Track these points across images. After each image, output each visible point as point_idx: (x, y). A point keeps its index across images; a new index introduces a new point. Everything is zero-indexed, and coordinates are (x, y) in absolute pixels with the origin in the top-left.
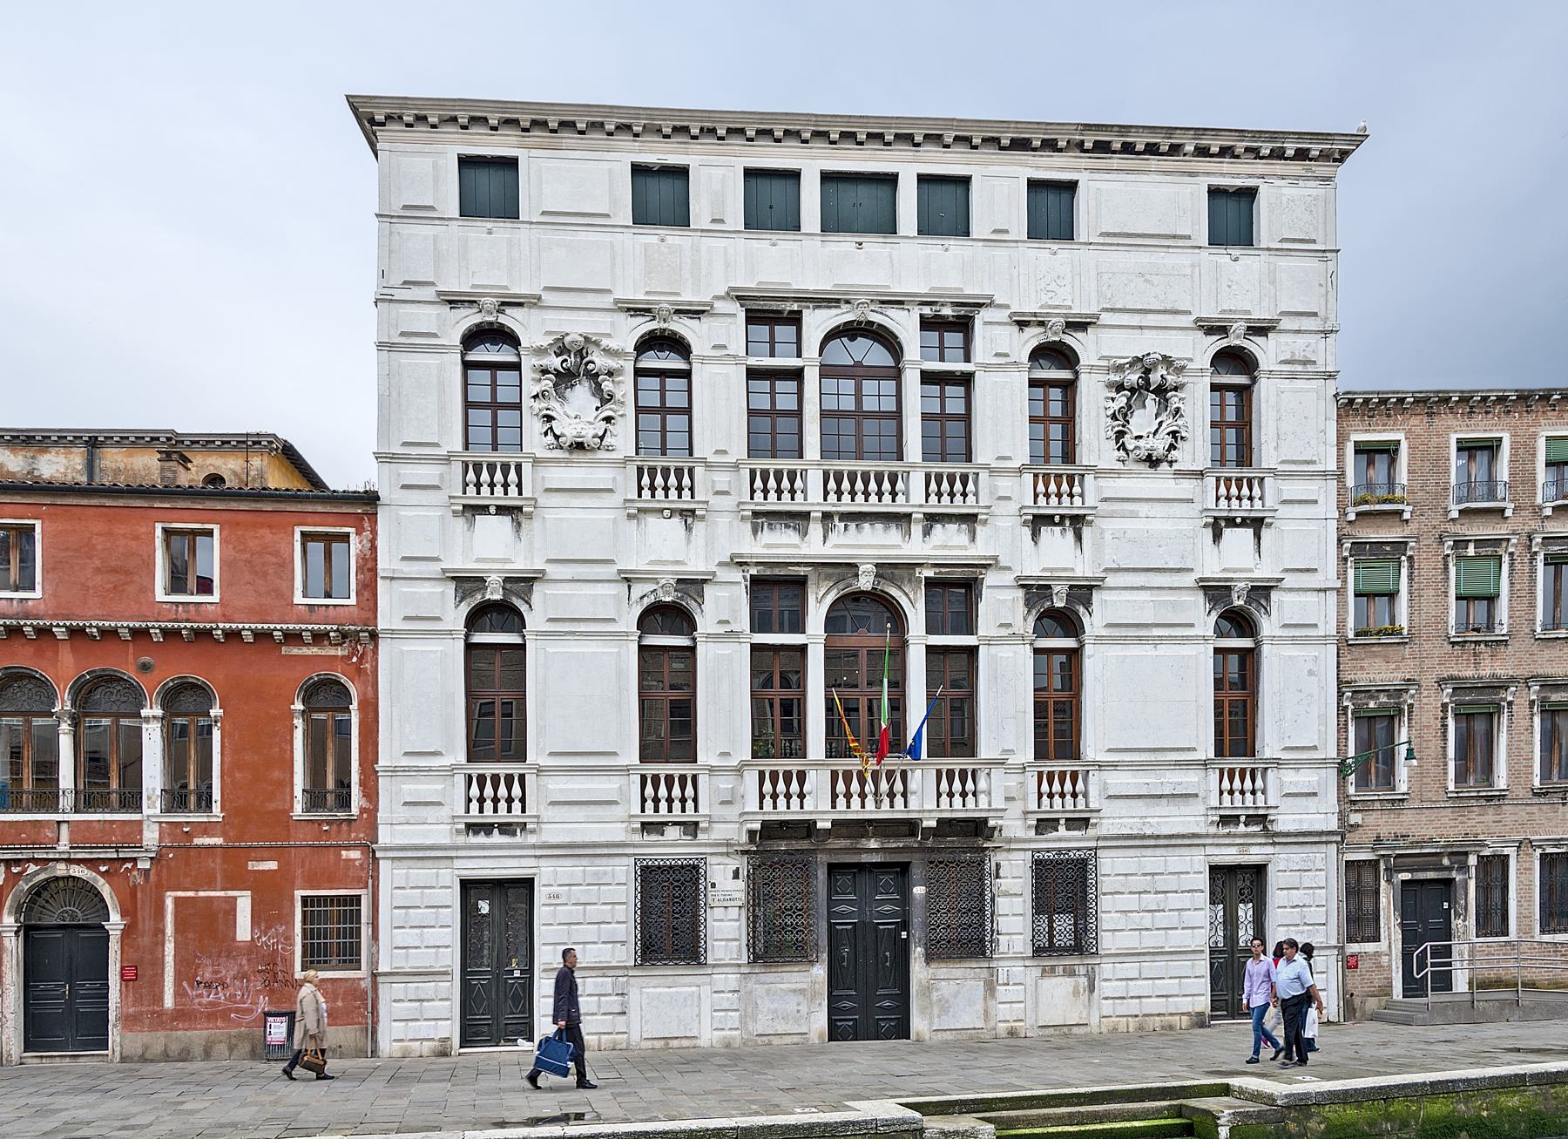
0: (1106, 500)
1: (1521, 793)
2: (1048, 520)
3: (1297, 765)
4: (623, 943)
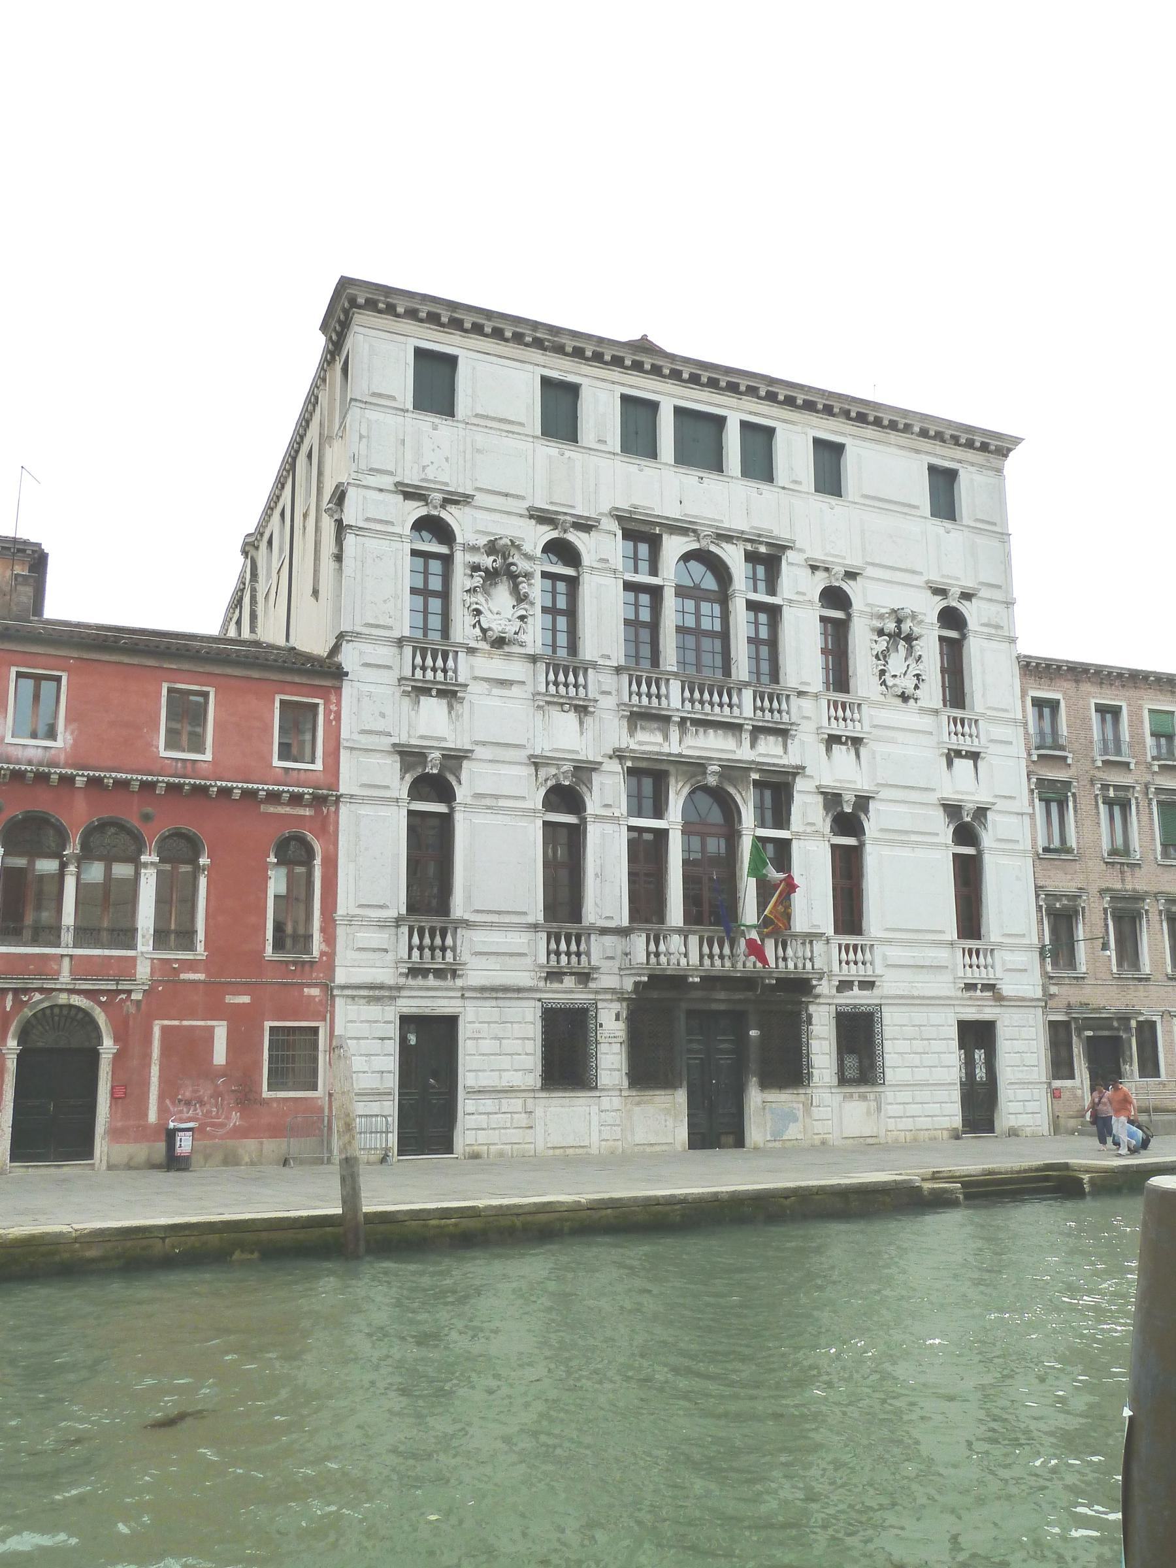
0: (875, 726)
1: (1161, 977)
2: (958, 754)
3: (1012, 948)
4: (531, 1071)
